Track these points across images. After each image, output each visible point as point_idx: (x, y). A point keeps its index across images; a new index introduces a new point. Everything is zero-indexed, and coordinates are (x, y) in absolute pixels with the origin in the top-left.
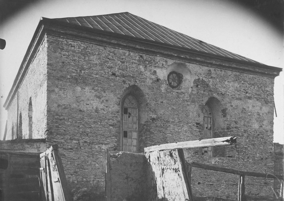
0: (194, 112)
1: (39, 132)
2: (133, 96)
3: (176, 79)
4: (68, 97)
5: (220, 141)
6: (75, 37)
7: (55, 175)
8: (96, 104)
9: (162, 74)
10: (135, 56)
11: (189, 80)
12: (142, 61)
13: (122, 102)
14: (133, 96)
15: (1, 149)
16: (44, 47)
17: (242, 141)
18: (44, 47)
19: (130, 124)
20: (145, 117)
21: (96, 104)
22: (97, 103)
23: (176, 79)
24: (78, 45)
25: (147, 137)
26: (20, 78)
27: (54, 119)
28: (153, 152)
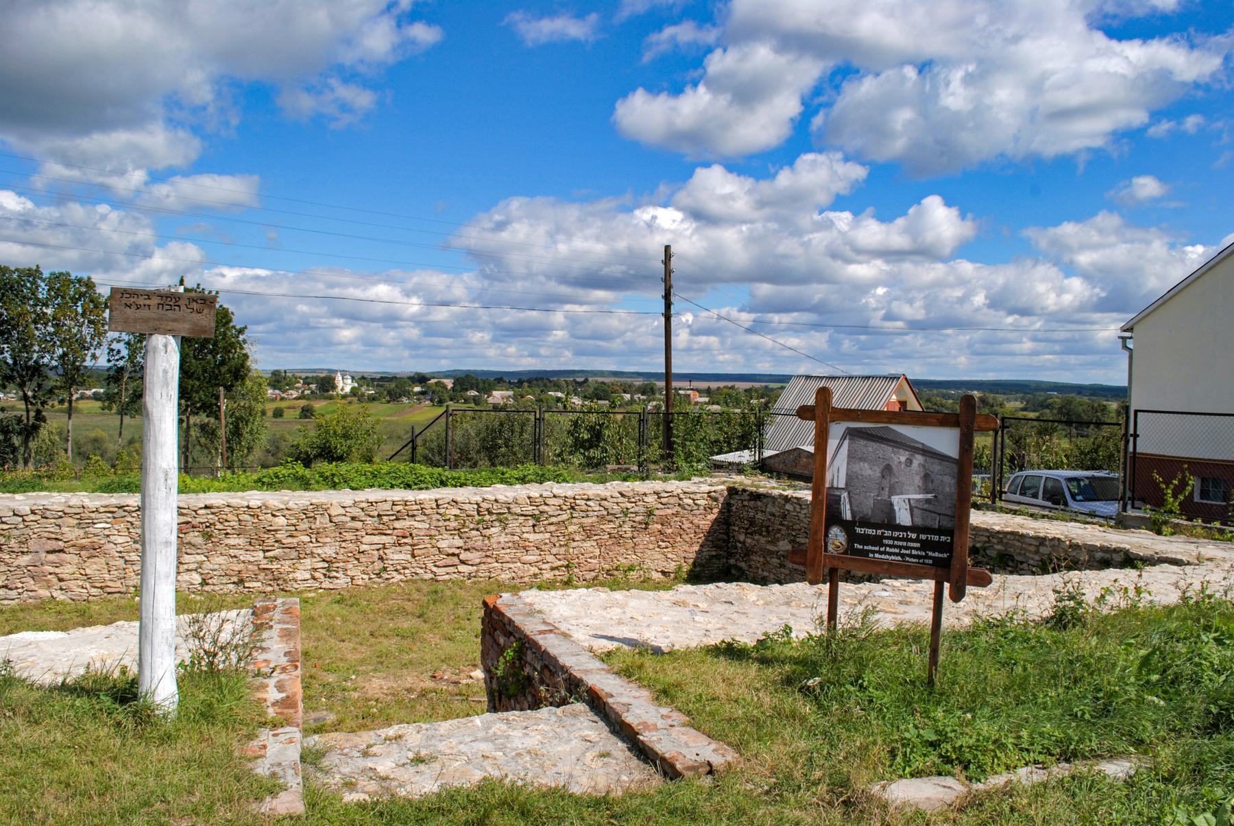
0: (918, 481)
1: (842, 485)
2: (887, 470)
3: (909, 462)
4: (856, 467)
5: (930, 496)
6: (862, 438)
7: (848, 507)
8: (869, 472)
9: (903, 459)
10: (890, 449)
11: (916, 463)
12: (893, 452)
13: (882, 472)
14: (887, 470)
15: (3, 410)
16: (846, 442)
17: (940, 497)
18: (846, 442)
19: (886, 483)
20: (893, 480)
21: (869, 472)
22: (869, 471)
23: (909, 462)
24: (863, 442)
25: (892, 492)
26: (1001, 536)
27: (849, 478)
28: (895, 499)
